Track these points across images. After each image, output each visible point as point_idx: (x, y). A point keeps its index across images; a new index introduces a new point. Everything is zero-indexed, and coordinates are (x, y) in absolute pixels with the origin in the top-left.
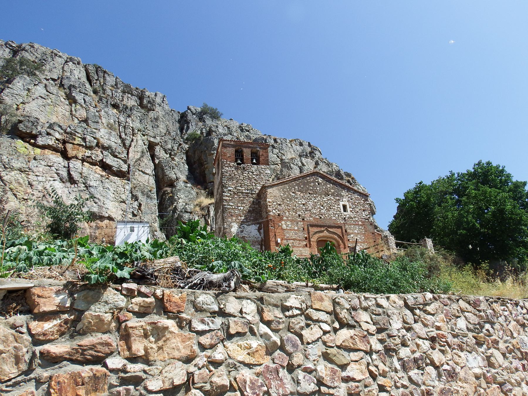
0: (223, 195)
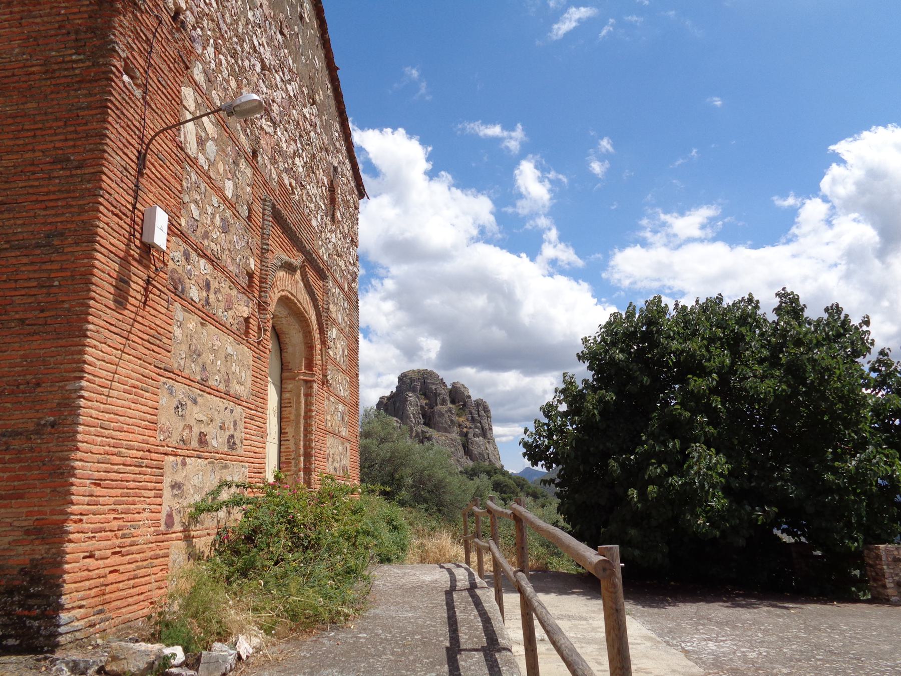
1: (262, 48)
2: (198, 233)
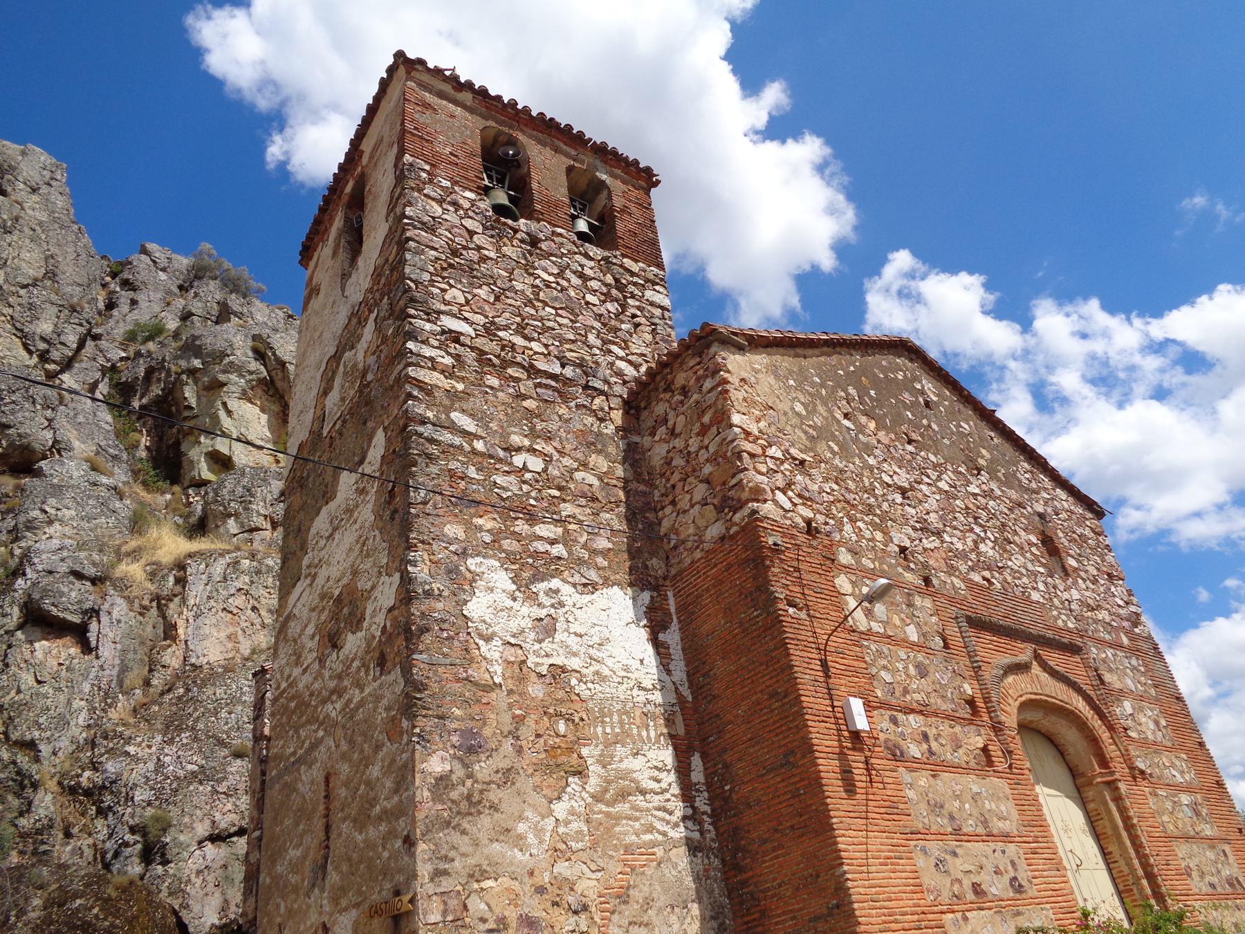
0: (402, 353)
1: (895, 477)
2: (897, 694)
